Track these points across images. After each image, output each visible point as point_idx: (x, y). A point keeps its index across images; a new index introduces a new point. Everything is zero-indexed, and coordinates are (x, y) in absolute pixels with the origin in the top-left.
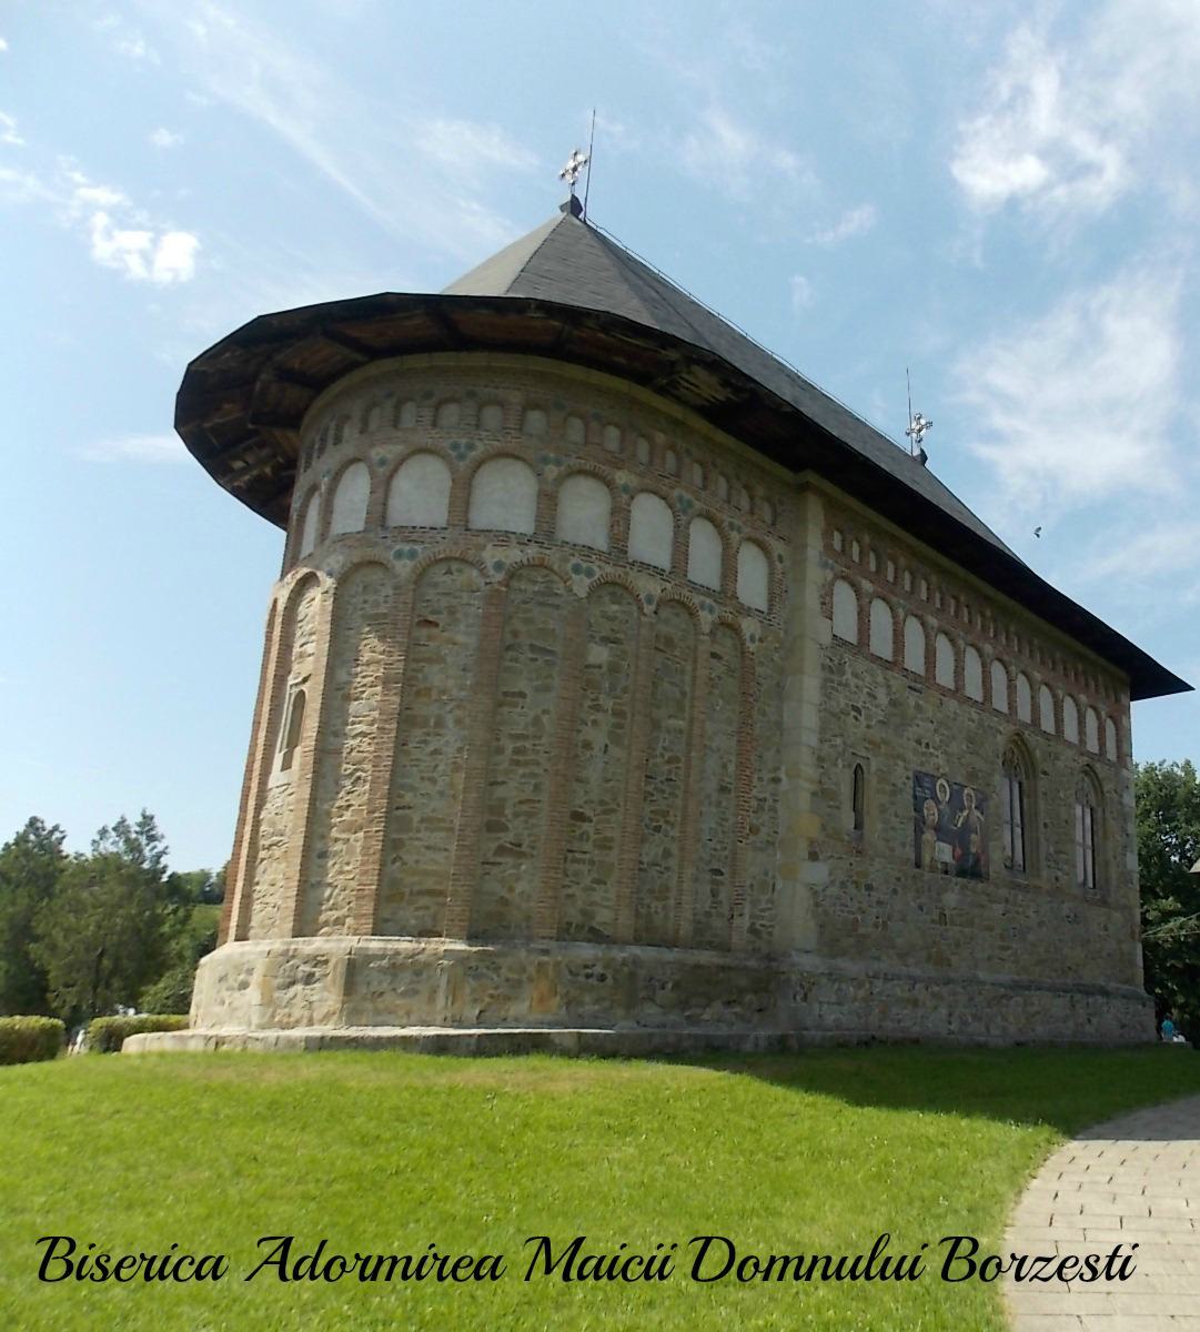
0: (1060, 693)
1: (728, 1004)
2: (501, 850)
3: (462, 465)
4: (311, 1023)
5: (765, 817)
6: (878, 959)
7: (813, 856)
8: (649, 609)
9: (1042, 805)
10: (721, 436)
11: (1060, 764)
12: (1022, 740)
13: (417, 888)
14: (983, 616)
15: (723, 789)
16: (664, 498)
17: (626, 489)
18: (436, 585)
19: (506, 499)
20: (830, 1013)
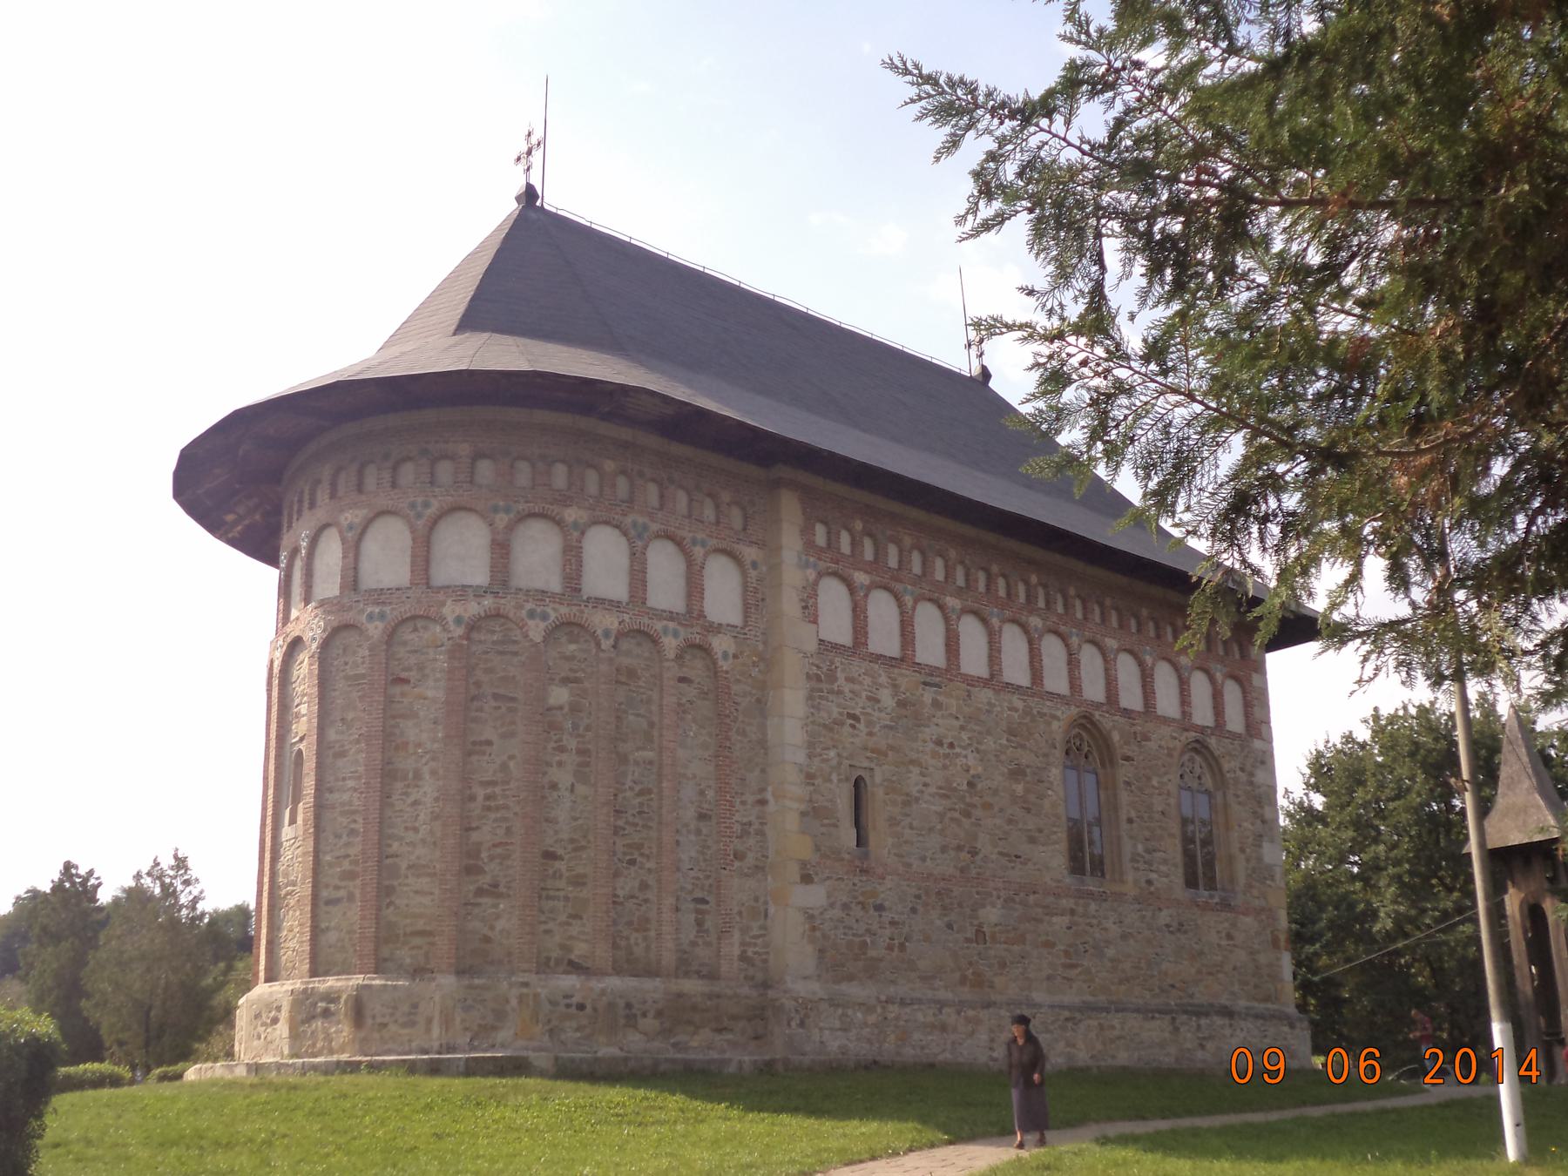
0: (1148, 659)
1: (719, 1031)
2: (480, 892)
3: (420, 523)
4: (331, 1052)
5: (751, 842)
6: (893, 982)
7: (807, 879)
8: (606, 644)
9: (1124, 797)
10: (678, 449)
11: (1152, 745)
12: (1093, 723)
13: (408, 930)
14: (1027, 583)
15: (702, 817)
16: (617, 527)
17: (576, 525)
18: (405, 643)
19: (464, 553)
20: (832, 1039)
